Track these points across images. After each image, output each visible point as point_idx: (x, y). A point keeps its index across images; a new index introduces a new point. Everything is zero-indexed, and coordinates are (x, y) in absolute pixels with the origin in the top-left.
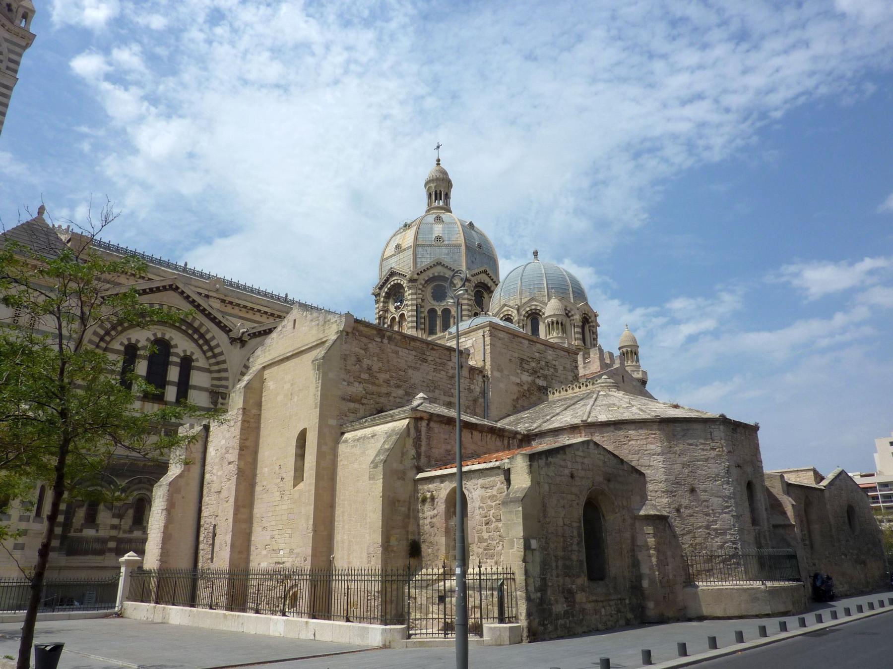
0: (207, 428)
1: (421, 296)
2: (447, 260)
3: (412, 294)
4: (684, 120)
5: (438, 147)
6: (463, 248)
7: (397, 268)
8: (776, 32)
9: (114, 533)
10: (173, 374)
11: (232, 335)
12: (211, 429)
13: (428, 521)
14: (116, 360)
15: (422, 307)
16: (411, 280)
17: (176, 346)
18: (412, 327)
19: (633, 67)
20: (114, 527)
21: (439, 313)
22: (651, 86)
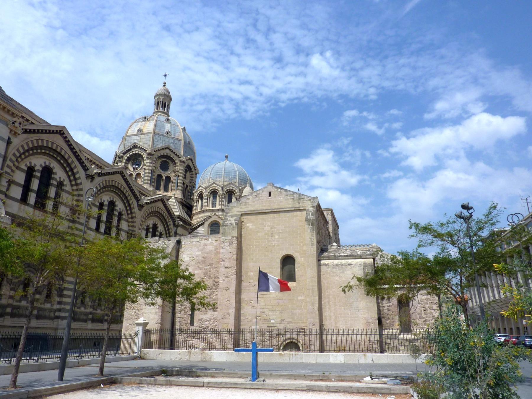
0: (179, 243)
1: (154, 165)
2: (173, 147)
3: (149, 163)
4: (239, 92)
5: (166, 75)
6: (183, 142)
7: (140, 144)
8: (294, 64)
9: (10, 301)
10: (52, 192)
11: (89, 172)
12: (183, 243)
13: (386, 308)
14: (20, 177)
15: (154, 172)
16: (150, 154)
17: (55, 173)
18: (147, 183)
19: (220, 55)
20: (11, 297)
21: (164, 178)
22: (227, 68)
